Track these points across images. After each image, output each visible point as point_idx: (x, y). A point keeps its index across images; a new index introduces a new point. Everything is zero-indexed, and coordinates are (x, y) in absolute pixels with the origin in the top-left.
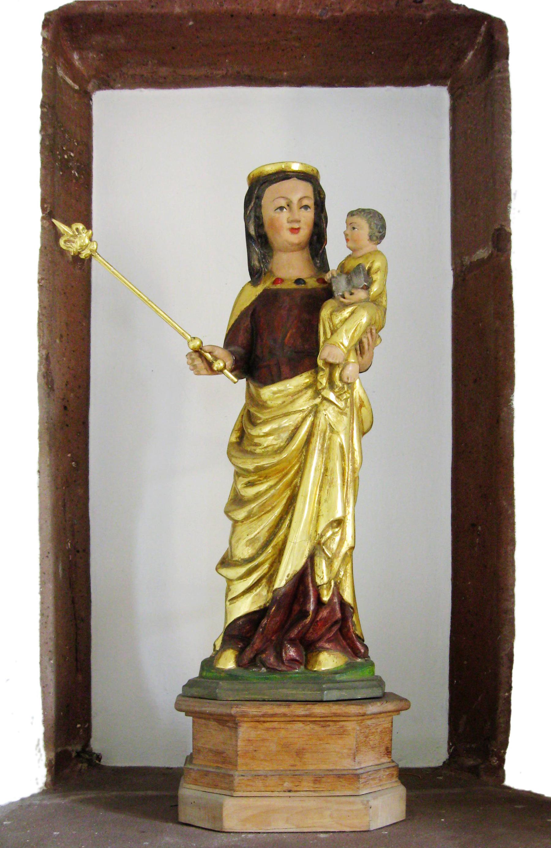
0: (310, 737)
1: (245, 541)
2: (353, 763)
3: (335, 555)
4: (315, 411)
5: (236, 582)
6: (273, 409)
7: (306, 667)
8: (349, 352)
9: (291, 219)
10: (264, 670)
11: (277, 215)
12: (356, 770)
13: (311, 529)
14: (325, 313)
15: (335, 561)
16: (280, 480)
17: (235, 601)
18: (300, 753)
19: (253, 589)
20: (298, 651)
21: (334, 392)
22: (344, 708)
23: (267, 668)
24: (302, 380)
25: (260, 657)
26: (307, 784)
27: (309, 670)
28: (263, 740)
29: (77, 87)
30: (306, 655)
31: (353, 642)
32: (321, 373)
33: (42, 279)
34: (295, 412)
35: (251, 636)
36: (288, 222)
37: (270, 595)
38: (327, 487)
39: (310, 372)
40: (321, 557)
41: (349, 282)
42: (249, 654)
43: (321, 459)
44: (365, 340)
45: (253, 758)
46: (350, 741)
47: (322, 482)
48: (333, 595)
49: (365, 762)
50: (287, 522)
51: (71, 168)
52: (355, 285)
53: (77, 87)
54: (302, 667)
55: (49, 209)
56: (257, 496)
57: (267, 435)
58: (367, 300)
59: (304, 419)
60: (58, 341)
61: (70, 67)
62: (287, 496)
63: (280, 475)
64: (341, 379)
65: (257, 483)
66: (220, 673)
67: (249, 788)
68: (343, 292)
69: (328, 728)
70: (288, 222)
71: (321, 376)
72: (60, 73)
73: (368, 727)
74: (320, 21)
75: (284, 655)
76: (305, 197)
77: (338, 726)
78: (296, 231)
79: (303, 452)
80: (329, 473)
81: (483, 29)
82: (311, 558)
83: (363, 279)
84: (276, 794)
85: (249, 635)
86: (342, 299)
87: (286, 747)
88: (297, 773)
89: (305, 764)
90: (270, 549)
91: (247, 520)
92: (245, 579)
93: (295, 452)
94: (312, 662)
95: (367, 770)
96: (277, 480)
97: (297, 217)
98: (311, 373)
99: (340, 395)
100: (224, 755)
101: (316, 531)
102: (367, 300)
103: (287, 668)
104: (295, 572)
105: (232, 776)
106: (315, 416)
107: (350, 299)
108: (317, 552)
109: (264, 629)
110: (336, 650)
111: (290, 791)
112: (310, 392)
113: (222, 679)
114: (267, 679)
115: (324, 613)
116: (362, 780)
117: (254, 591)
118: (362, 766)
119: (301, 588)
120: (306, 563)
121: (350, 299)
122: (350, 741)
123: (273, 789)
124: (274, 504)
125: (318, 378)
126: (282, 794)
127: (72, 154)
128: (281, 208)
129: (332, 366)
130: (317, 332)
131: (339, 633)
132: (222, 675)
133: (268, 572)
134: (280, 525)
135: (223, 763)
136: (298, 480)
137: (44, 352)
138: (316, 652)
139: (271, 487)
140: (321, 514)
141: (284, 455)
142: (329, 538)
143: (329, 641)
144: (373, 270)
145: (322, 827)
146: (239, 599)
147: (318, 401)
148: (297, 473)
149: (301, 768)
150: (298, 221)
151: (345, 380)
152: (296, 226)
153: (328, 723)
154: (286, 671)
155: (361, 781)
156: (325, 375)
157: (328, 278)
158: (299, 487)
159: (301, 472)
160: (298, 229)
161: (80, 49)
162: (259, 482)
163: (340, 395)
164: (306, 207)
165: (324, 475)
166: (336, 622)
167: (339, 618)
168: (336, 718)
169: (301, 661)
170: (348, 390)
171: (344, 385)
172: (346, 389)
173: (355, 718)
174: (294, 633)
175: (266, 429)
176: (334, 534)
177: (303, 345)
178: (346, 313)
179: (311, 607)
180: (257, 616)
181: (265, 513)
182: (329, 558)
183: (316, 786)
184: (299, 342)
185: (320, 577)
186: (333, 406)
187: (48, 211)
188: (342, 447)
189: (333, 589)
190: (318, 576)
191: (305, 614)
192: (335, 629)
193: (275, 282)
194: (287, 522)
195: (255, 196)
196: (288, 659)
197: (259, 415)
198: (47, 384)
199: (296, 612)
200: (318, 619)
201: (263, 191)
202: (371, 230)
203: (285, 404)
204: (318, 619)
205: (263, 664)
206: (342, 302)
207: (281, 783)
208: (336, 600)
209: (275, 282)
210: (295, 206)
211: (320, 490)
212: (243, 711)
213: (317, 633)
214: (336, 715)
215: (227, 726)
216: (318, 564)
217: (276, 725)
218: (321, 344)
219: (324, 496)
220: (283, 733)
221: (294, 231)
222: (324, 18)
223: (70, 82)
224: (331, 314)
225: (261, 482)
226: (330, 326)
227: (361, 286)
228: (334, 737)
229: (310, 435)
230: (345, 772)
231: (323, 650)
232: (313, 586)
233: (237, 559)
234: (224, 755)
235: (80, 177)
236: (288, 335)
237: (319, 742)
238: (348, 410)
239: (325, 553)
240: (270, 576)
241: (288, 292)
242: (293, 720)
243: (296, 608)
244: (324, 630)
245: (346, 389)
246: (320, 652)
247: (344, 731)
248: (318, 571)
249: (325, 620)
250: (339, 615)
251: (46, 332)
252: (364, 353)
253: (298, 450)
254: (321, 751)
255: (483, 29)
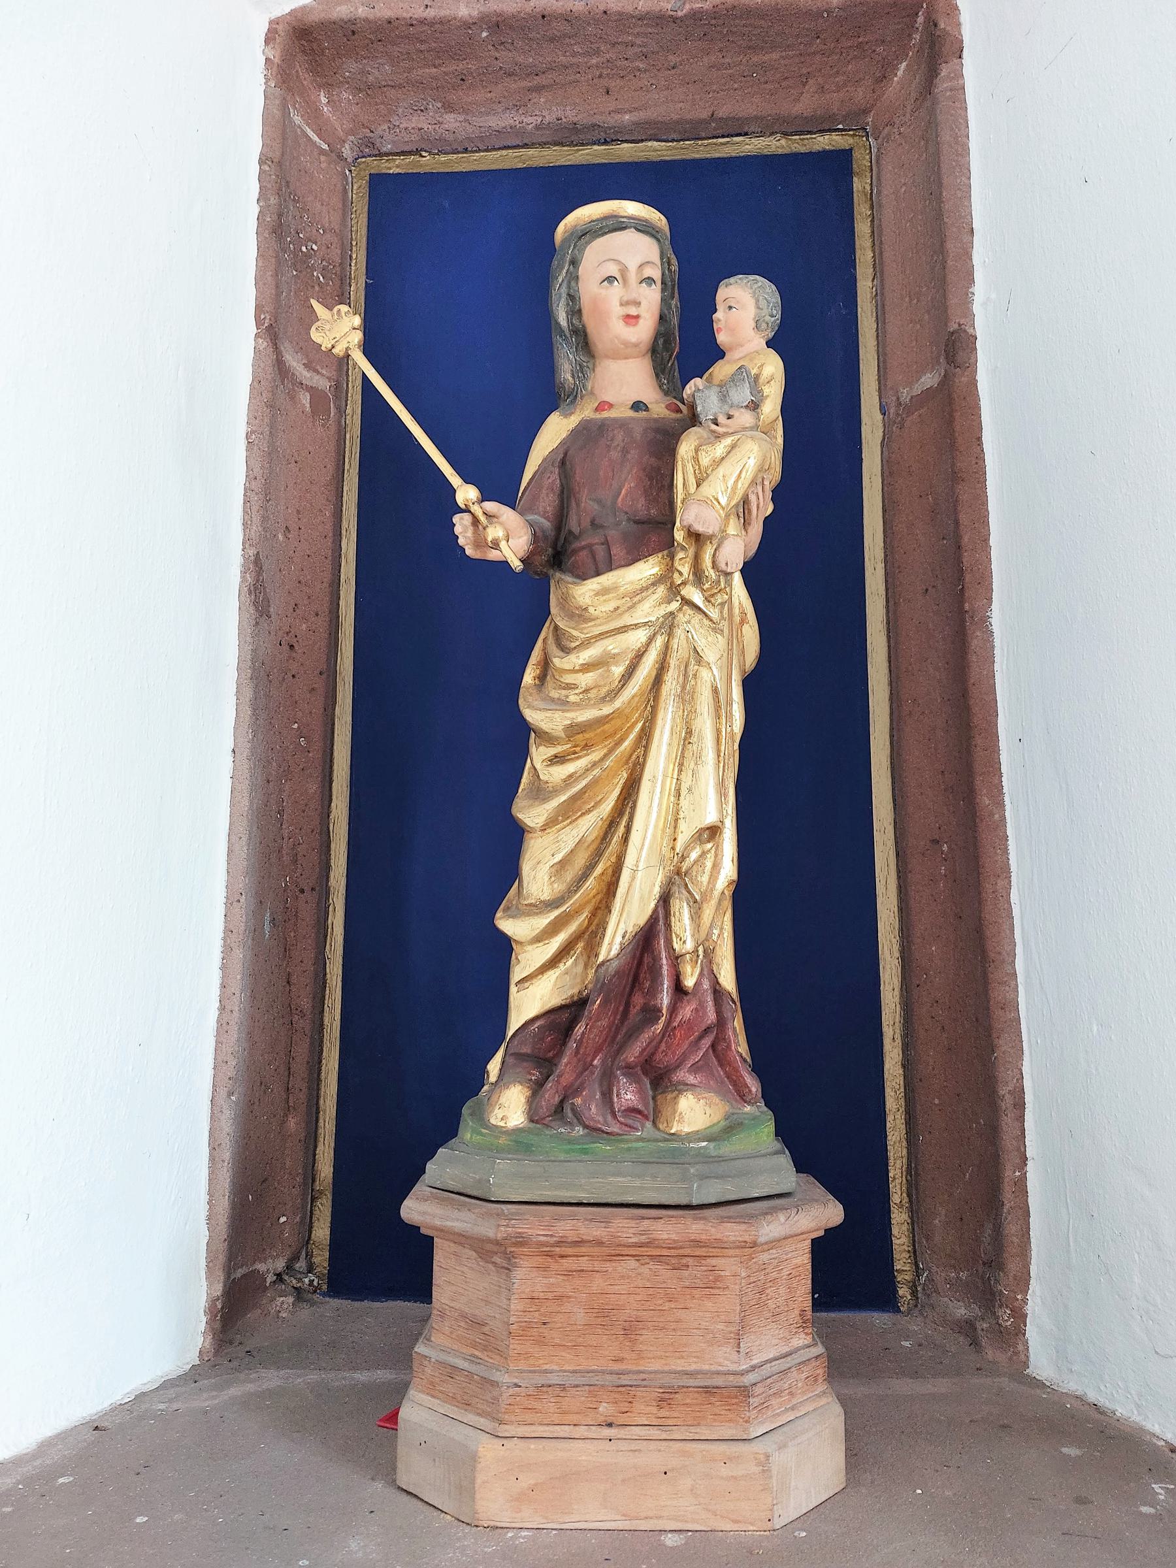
0: (651, 1291)
1: (548, 866)
2: (735, 1356)
3: (705, 896)
4: (669, 624)
5: (529, 948)
6: (598, 622)
7: (654, 1123)
8: (727, 516)
9: (625, 299)
10: (579, 1131)
11: (603, 292)
12: (742, 1373)
13: (665, 845)
14: (685, 449)
15: (705, 906)
16: (610, 752)
17: (526, 985)
18: (630, 1330)
19: (560, 961)
20: (641, 1092)
21: (703, 590)
22: (713, 1230)
23: (586, 1127)
24: (647, 569)
25: (573, 1104)
26: (644, 1410)
27: (659, 1129)
28: (560, 1298)
29: (325, 147)
30: (654, 1098)
31: (737, 1070)
32: (681, 555)
33: (252, 432)
34: (636, 626)
35: (556, 1056)
36: (621, 305)
37: (591, 973)
38: (692, 764)
39: (660, 555)
40: (681, 899)
41: (724, 397)
42: (550, 1094)
43: (681, 713)
44: (753, 498)
45: (541, 1342)
46: (729, 1302)
47: (683, 756)
48: (701, 974)
49: (760, 1351)
50: (621, 829)
51: (313, 269)
52: (736, 402)
53: (325, 147)
54: (649, 1125)
55: (267, 321)
56: (570, 780)
57: (586, 668)
58: (755, 427)
59: (651, 640)
60: (280, 537)
61: (313, 115)
62: (622, 781)
63: (610, 743)
64: (714, 565)
65: (569, 757)
66: (497, 1138)
67: (529, 1417)
68: (716, 414)
69: (686, 1273)
70: (621, 305)
71: (681, 559)
72: (297, 120)
73: (763, 1268)
74: (674, 20)
75: (615, 1100)
76: (648, 262)
77: (704, 1268)
78: (634, 320)
79: (649, 700)
80: (694, 739)
81: (920, 19)
82: (665, 900)
83: (748, 392)
84: (581, 1431)
85: (551, 1054)
86: (714, 427)
87: (603, 1315)
88: (625, 1380)
89: (640, 1357)
90: (590, 882)
91: (550, 828)
92: (547, 942)
93: (636, 699)
94: (666, 1112)
95: (767, 1370)
96: (605, 751)
97: (633, 295)
98: (663, 557)
99: (712, 596)
100: (486, 1329)
101: (673, 848)
102: (755, 427)
103: (620, 1129)
104: (637, 929)
105: (494, 1384)
106: (670, 634)
107: (726, 426)
108: (675, 889)
109: (580, 1043)
110: (709, 1089)
111: (610, 1425)
112: (661, 590)
113: (500, 1150)
114: (585, 1152)
115: (687, 1011)
116: (754, 1400)
117: (561, 965)
118: (755, 1362)
119: (647, 959)
120: (655, 911)
121: (726, 426)
122: (729, 1302)
123: (574, 1418)
124: (600, 797)
125: (676, 564)
126: (595, 1432)
127: (315, 247)
128: (610, 279)
129: (697, 538)
130: (671, 485)
131: (711, 1051)
132: (503, 1141)
133: (587, 928)
134: (609, 836)
135: (485, 1349)
136: (641, 751)
137: (252, 552)
138: (673, 1091)
139: (594, 764)
140: (681, 815)
141: (618, 703)
142: (696, 862)
143: (695, 1068)
144: (762, 380)
145: (675, 1519)
146: (534, 981)
147: (674, 606)
148: (639, 738)
149: (635, 1368)
150: (638, 304)
151: (723, 566)
152: (633, 311)
153: (684, 1261)
154: (618, 1134)
155: (754, 1401)
156: (688, 559)
157: (689, 393)
158: (643, 766)
159: (645, 737)
160: (637, 317)
161: (328, 86)
162: (573, 756)
163: (712, 596)
164: (650, 280)
165: (687, 742)
166: (707, 1030)
167: (712, 1023)
168: (701, 1249)
169: (646, 1112)
170: (725, 588)
171: (719, 576)
172: (723, 585)
173: (737, 1252)
174: (633, 1052)
175: (585, 656)
176: (703, 854)
177: (648, 509)
178: (720, 449)
179: (665, 999)
180: (565, 1015)
181: (583, 814)
182: (695, 901)
183: (663, 1413)
184: (641, 503)
185: (681, 940)
186: (700, 616)
187: (266, 325)
188: (715, 691)
189: (702, 962)
190: (677, 936)
191: (651, 1013)
192: (707, 1042)
193: (600, 407)
194: (621, 829)
195: (568, 258)
196: (623, 1108)
197: (575, 633)
198: (255, 603)
199: (638, 1008)
200: (676, 1024)
201: (582, 251)
202: (759, 311)
203: (619, 611)
204: (676, 1024)
205: (579, 1118)
206: (713, 432)
207: (591, 1406)
208: (706, 985)
209: (600, 407)
210: (633, 277)
211: (680, 771)
212: (520, 1233)
213: (674, 1053)
214: (697, 1243)
215: (493, 1263)
216: (677, 913)
217: (584, 1263)
218: (679, 504)
219: (686, 780)
220: (598, 1283)
221: (631, 319)
222: (680, 14)
223: (315, 138)
224: (697, 450)
225: (576, 755)
226: (695, 471)
227: (745, 404)
228: (696, 1292)
229: (662, 668)
230: (719, 1381)
231: (686, 1088)
232: (669, 957)
233: (533, 901)
234: (486, 1329)
235: (328, 284)
236: (623, 492)
237: (667, 1306)
238: (725, 625)
239: (689, 892)
240: (592, 934)
241: (622, 424)
242: (616, 1252)
243: (638, 1000)
244: (685, 1046)
245: (723, 585)
246: (680, 1092)
247: (716, 1280)
248: (676, 926)
249: (689, 1025)
250: (711, 1016)
251: (257, 519)
252: (749, 524)
253: (642, 695)
254: (673, 1326)
255: (920, 19)
